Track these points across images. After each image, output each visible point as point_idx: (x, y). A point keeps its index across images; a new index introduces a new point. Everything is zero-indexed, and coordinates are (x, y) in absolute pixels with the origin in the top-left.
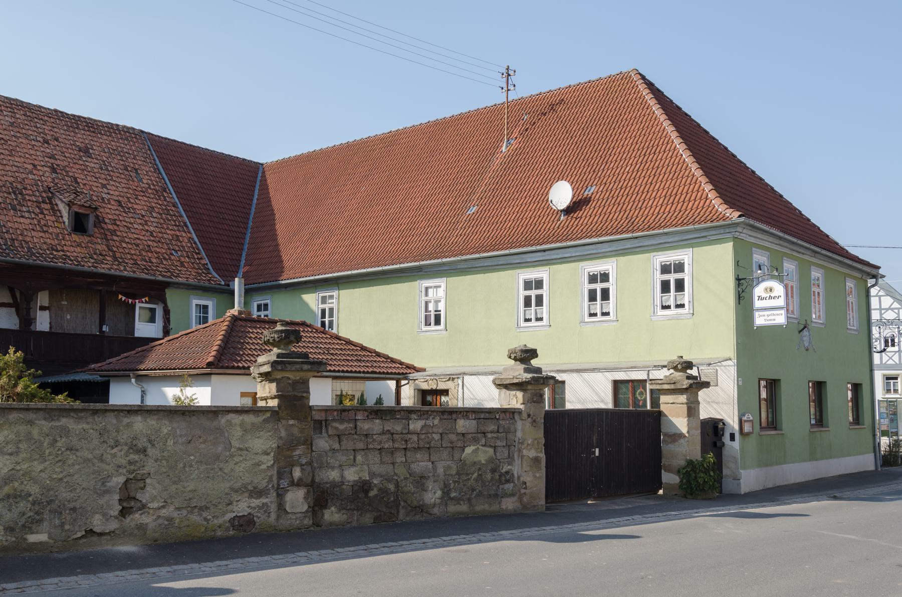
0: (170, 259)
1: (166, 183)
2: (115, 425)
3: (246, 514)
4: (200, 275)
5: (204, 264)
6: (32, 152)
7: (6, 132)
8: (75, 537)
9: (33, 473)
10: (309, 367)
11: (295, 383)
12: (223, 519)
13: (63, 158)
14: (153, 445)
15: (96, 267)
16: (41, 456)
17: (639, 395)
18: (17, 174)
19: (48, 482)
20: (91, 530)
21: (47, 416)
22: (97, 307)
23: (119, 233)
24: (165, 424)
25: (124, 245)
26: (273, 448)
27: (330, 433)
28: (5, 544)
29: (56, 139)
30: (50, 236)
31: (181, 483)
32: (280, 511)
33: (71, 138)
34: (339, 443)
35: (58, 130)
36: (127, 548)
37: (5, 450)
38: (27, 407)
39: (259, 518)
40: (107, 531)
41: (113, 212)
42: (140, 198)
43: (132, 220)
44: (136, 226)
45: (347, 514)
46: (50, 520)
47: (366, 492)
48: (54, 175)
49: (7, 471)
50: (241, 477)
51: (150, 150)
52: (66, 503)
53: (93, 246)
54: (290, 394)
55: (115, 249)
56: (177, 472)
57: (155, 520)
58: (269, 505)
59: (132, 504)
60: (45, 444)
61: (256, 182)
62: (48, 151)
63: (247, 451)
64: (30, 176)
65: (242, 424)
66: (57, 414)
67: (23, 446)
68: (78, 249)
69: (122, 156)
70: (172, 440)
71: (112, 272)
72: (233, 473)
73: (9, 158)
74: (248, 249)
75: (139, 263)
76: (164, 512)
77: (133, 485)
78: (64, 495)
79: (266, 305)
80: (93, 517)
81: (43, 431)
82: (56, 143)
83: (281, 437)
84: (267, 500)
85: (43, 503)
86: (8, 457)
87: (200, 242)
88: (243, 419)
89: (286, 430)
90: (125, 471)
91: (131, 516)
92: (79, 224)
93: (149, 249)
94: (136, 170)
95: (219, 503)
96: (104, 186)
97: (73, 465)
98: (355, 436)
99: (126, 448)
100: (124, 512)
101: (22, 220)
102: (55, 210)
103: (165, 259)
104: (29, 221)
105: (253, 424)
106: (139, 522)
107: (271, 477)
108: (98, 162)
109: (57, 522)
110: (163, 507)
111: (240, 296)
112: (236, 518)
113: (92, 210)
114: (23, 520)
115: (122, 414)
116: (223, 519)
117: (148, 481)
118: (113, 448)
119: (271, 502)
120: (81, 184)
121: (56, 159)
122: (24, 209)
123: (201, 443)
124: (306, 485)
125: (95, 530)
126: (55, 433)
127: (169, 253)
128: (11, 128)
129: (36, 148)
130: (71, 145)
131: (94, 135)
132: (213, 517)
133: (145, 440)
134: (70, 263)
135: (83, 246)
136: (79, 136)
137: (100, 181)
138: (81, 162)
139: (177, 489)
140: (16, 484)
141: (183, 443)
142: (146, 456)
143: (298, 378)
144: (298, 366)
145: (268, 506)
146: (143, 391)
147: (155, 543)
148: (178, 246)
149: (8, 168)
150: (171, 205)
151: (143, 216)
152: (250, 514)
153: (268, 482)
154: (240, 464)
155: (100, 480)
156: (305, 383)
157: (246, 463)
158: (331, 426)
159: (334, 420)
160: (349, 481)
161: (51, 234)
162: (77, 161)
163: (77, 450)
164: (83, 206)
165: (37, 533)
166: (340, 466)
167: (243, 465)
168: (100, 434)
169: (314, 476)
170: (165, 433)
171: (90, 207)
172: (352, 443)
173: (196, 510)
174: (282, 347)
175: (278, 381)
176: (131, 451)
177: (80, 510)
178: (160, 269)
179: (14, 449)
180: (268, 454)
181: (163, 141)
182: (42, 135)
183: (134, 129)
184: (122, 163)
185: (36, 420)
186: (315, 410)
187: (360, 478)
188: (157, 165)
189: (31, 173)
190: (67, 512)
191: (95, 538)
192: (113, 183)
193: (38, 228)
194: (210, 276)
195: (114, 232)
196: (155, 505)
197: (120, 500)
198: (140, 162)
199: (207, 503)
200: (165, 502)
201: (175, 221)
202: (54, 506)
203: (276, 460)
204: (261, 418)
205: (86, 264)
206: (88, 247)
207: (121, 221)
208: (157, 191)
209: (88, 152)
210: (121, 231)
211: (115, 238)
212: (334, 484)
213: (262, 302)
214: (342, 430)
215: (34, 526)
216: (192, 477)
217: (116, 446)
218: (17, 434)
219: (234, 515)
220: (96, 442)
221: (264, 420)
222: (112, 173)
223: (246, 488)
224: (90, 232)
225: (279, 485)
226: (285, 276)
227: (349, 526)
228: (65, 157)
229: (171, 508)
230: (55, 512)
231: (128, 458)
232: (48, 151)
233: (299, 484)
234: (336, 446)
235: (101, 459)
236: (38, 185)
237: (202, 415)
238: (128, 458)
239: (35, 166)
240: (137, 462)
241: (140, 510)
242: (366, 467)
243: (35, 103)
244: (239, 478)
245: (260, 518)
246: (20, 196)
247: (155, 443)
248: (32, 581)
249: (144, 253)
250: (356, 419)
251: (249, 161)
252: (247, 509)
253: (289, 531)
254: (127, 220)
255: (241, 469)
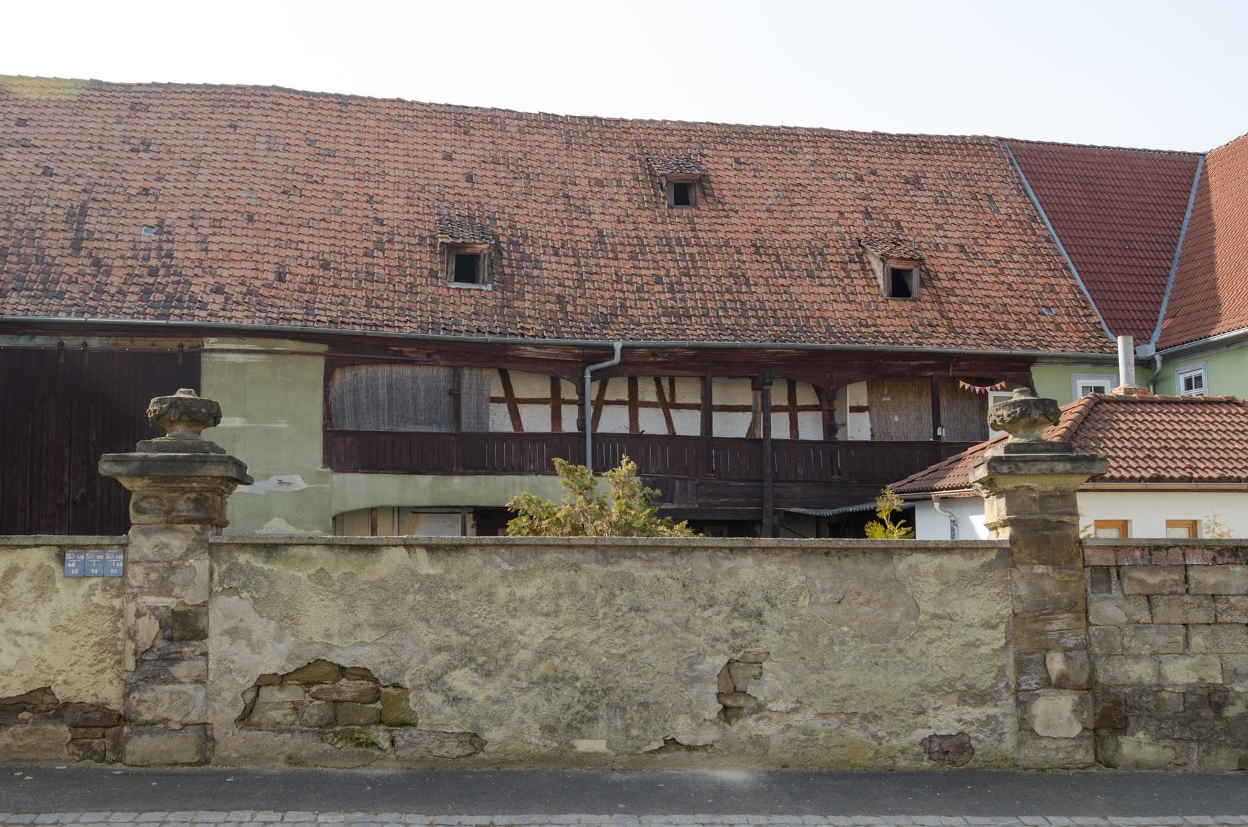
0: (1038, 321)
1: (1036, 209)
2: (708, 572)
3: (954, 733)
4: (1087, 340)
5: (1095, 323)
6: (838, 195)
7: (805, 175)
8: (648, 748)
9: (582, 645)
10: (1068, 466)
11: (1045, 498)
12: (908, 739)
13: (881, 197)
14: (773, 606)
15: (921, 344)
16: (593, 618)
17: (593, 373)
18: (817, 229)
19: (605, 660)
20: (674, 739)
21: (601, 556)
22: (927, 402)
23: (958, 292)
24: (795, 571)
25: (966, 308)
26: (1002, 617)
27: (1127, 590)
28: (544, 750)
29: (874, 173)
30: (858, 306)
31: (826, 672)
32: (1023, 732)
33: (895, 167)
34: (1151, 609)
35: (876, 160)
36: (733, 774)
37: (539, 608)
38: (566, 543)
39: (980, 741)
40: (701, 744)
41: (951, 262)
42: (993, 236)
43: (980, 270)
44: (985, 278)
45: (1174, 748)
46: (609, 719)
47: (1219, 707)
48: (868, 222)
49: (541, 640)
50: (941, 667)
51: (1012, 164)
52: (632, 693)
53: (918, 314)
54: (1035, 517)
55: (951, 315)
56: (818, 652)
57: (782, 732)
58: (1001, 719)
59: (742, 702)
60: (598, 601)
61: (1191, 185)
62: (861, 190)
63: (952, 620)
64: (835, 229)
65: (939, 573)
66: (616, 553)
67: (565, 603)
68: (897, 321)
69: (968, 180)
70: (807, 599)
71: (945, 349)
72: (924, 660)
73: (808, 208)
74: (1172, 292)
75: (987, 331)
76: (797, 719)
77: (740, 671)
78: (629, 681)
79: (1199, 379)
80: (675, 720)
81: (594, 581)
82: (873, 178)
83: (1019, 597)
84: (997, 709)
85: (597, 691)
86: (542, 619)
87: (1088, 290)
88: (941, 565)
89: (1029, 584)
90: (725, 646)
91: (741, 722)
92: (899, 286)
93: (1005, 308)
94: (990, 196)
95: (900, 710)
96: (939, 227)
97: (642, 634)
98: (1187, 598)
99: (727, 609)
100: (728, 714)
101: (821, 290)
102: (866, 270)
103: (1030, 322)
104: (829, 290)
105: (962, 574)
106: (753, 733)
107: (1002, 670)
108: (932, 194)
109: (619, 723)
110: (796, 710)
111: (1127, 364)
112: (935, 739)
113: (916, 263)
114: (568, 717)
115: (720, 554)
116: (908, 739)
117: (766, 665)
118: (705, 609)
119: (1005, 715)
120: (905, 229)
121: (872, 200)
122: (824, 274)
123: (861, 604)
124: (1077, 688)
125: (678, 740)
126: (612, 583)
127: (1036, 313)
128: (812, 169)
129: (844, 189)
130: (894, 176)
131: (927, 157)
132: (890, 734)
133: (759, 597)
134: (883, 341)
135: (905, 315)
136: (906, 162)
137: (934, 220)
138: (907, 199)
139: (818, 681)
140: (557, 661)
141: (826, 605)
142: (761, 623)
143: (1051, 488)
144: (1044, 466)
145: (997, 722)
146: (953, 522)
147: (784, 770)
148: (1053, 300)
149: (805, 222)
150: (1043, 239)
151: (997, 262)
152: (961, 733)
153: (995, 678)
154: (937, 643)
155: (685, 661)
156: (1067, 500)
157: (949, 641)
158: (1130, 578)
159: (1134, 566)
160: (1175, 685)
161: (860, 304)
162: (902, 198)
163: (647, 611)
164: (902, 258)
165: (590, 738)
166: (1154, 654)
167: (945, 645)
168: (684, 586)
169: (1093, 671)
170: (794, 586)
171: (911, 259)
172: (1180, 611)
173: (857, 719)
174: (1021, 432)
175: (1009, 495)
176: (736, 614)
177: (655, 707)
178: (1021, 338)
179: (551, 608)
180: (994, 627)
181: (1034, 147)
182: (854, 170)
183: (987, 138)
184: (967, 189)
185: (583, 563)
186: (1089, 547)
187: (1201, 679)
188: (1021, 184)
189: (837, 224)
190: (635, 708)
191: (682, 754)
192: (954, 221)
193: (842, 298)
194: (1104, 340)
195: (951, 292)
196: (779, 706)
197: (719, 695)
198: (996, 185)
199: (877, 708)
200: (798, 701)
201: (1048, 263)
202: (614, 698)
203: (1010, 638)
204: (977, 561)
205: (906, 341)
206: (912, 316)
207: (963, 273)
208: (1021, 222)
209: (919, 183)
210: (962, 289)
211: (953, 299)
212: (1141, 690)
213: (1193, 374)
214: (1154, 585)
215: (585, 727)
216: (844, 663)
217: (711, 606)
218: (556, 584)
219: (931, 732)
220: (676, 598)
221: (982, 566)
222: (952, 207)
223: (951, 686)
224: (915, 294)
225: (1018, 684)
226: (1225, 323)
227: (1179, 771)
228: (885, 194)
229: (810, 714)
230: (616, 707)
231: (731, 627)
232: (861, 190)
233: (1061, 684)
234: (1144, 616)
235: (686, 626)
236: (845, 239)
237: (861, 555)
238: (731, 627)
239: (841, 214)
240: (746, 632)
241: (754, 713)
242: (1215, 660)
243: (846, 129)
244: (937, 668)
245: (983, 743)
246: (819, 258)
247: (778, 602)
248: (539, 816)
249: (996, 317)
250: (1186, 566)
251: (1179, 153)
252: (956, 724)
253: (1043, 770)
254: (972, 270)
255: (941, 651)
